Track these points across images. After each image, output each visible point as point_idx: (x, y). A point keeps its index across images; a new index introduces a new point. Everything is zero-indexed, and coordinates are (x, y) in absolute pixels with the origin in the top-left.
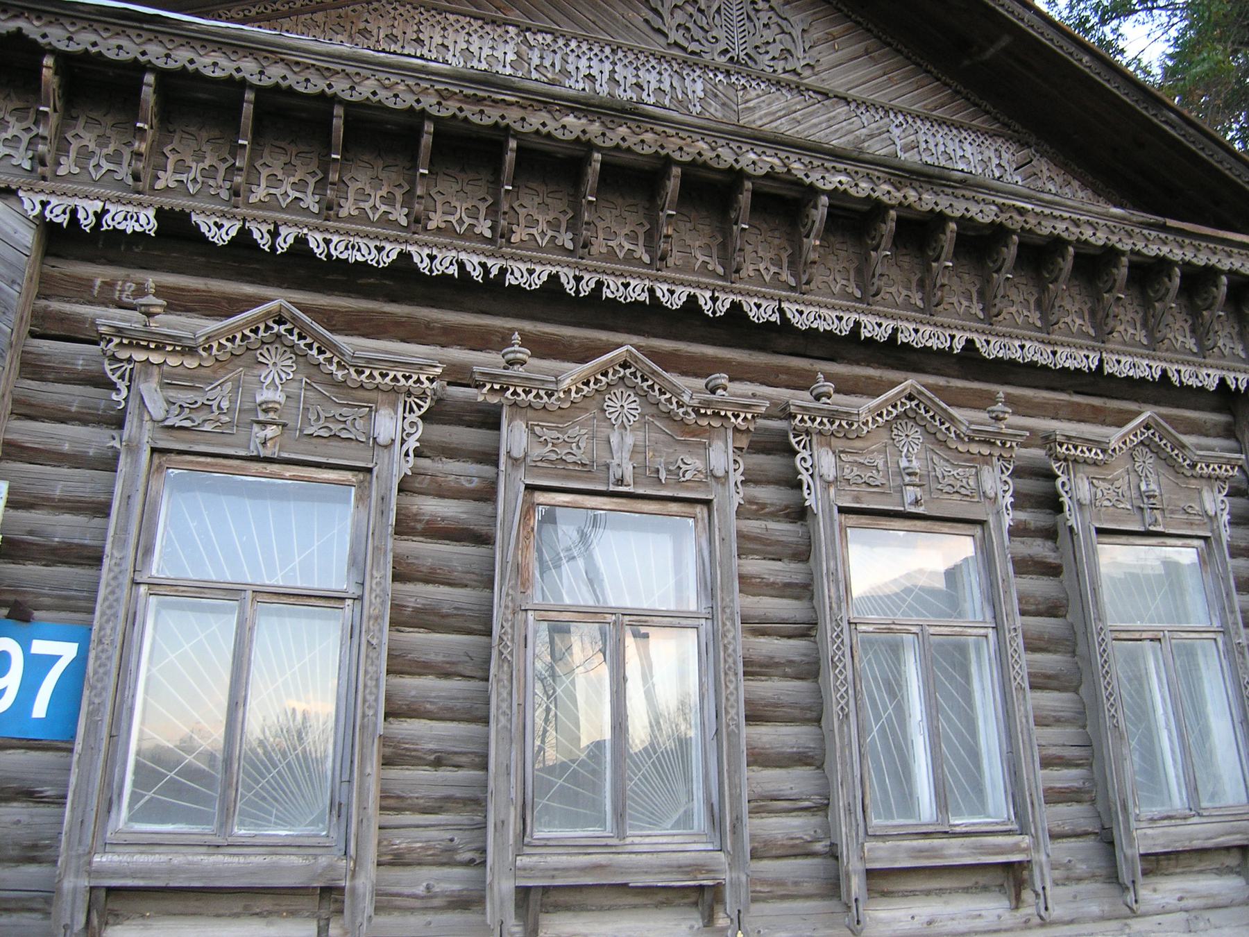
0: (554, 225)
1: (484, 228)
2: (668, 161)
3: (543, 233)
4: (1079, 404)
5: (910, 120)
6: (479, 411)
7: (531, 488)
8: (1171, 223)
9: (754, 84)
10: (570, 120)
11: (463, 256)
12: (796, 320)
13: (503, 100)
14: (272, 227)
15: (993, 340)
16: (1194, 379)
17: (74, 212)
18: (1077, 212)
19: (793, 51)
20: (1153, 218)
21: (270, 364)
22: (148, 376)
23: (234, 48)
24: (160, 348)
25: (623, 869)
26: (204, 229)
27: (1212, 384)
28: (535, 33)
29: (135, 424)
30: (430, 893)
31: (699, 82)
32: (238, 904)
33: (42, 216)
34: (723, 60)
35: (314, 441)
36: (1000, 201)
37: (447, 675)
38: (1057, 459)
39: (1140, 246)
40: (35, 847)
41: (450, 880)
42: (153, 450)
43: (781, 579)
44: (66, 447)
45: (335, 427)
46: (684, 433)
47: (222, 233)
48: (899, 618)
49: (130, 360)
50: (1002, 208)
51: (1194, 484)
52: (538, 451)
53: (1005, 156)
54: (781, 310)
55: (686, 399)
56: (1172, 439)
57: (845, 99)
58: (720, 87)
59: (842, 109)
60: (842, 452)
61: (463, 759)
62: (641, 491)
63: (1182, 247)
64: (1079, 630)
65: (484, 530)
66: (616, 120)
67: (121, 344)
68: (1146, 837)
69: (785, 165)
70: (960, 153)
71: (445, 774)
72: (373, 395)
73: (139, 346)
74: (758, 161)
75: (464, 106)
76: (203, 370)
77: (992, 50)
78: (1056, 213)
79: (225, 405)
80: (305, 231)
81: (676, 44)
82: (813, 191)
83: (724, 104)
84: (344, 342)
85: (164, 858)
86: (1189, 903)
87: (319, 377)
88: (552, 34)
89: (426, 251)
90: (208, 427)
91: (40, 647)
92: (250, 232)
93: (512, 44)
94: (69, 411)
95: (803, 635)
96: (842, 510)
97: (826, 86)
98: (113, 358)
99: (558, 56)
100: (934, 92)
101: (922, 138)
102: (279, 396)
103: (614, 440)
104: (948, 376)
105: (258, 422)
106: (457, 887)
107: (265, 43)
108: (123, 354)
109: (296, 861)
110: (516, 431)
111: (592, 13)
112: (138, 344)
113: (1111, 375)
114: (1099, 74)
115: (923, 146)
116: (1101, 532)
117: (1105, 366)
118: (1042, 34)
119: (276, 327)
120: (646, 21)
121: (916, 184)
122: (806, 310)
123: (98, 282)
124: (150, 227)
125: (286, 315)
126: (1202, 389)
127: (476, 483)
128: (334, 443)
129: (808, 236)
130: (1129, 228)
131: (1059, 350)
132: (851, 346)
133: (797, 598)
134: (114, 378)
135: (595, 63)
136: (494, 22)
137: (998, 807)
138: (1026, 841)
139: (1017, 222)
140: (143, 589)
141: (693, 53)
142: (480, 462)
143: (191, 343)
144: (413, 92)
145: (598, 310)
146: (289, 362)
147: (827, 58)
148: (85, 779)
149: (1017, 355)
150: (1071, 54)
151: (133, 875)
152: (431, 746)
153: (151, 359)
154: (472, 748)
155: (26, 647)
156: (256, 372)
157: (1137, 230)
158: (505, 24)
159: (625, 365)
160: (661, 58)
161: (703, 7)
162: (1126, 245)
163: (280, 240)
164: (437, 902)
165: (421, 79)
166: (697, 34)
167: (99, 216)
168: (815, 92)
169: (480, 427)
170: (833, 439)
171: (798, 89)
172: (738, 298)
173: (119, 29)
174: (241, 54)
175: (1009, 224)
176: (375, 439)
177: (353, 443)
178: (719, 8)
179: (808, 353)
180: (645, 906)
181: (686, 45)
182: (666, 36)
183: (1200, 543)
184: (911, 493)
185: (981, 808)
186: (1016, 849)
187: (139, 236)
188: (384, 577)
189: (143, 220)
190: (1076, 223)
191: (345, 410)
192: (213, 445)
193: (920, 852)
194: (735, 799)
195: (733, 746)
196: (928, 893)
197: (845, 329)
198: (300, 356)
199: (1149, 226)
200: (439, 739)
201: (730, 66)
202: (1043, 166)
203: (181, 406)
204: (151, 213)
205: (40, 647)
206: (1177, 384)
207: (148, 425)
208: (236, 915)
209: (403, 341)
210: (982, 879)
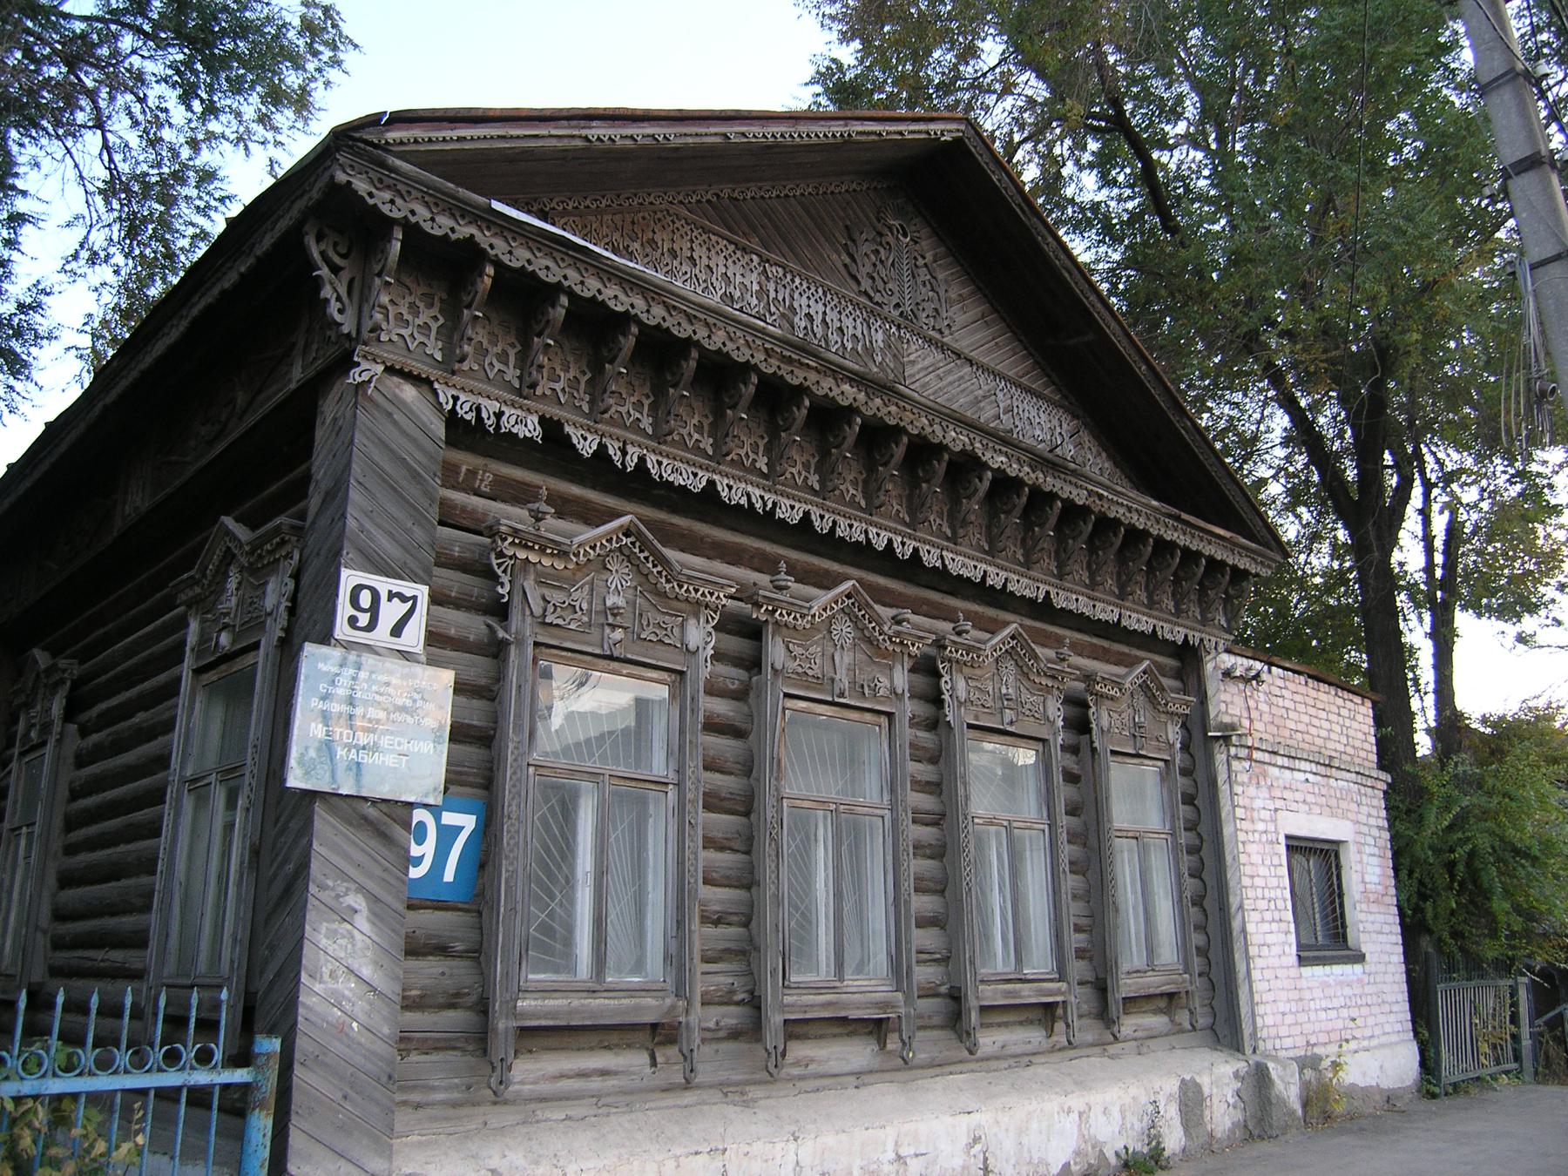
0: (806, 466)
7: (786, 695)
10: (846, 387)
11: (750, 488)
17: (478, 410)
24: (542, 550)
25: (845, 1006)
26: (575, 441)
30: (718, 1027)
32: (594, 1039)
33: (453, 411)
37: (722, 849)
40: (457, 995)
41: (731, 1016)
42: (536, 644)
43: (925, 778)
44: (453, 631)
45: (661, 633)
47: (587, 446)
48: (997, 814)
50: (1090, 493)
51: (1163, 718)
52: (792, 665)
53: (1065, 426)
55: (886, 628)
59: (967, 369)
61: (735, 918)
62: (853, 703)
64: (755, 751)
65: (744, 726)
67: (512, 543)
68: (537, 995)
71: (722, 930)
72: (683, 606)
73: (526, 547)
74: (957, 439)
81: (866, 293)
82: (985, 466)
84: (671, 554)
85: (565, 1002)
86: (1139, 1034)
87: (647, 586)
89: (726, 481)
91: (449, 818)
93: (755, 275)
95: (935, 824)
96: (970, 726)
98: (501, 555)
100: (1024, 359)
102: (621, 602)
103: (837, 658)
106: (734, 1021)
107: (656, 286)
109: (650, 1001)
116: (1113, 753)
120: (845, 266)
123: (464, 469)
126: (1174, 642)
127: (735, 686)
128: (659, 647)
133: (931, 793)
134: (499, 572)
135: (812, 302)
137: (1040, 961)
138: (1063, 986)
139: (1097, 506)
140: (531, 769)
145: (831, 545)
148: (166, 924)
149: (1073, 607)
151: (546, 1016)
152: (717, 908)
154: (742, 909)
155: (438, 819)
159: (849, 596)
160: (857, 305)
164: (721, 1034)
173: (548, 250)
180: (841, 1035)
182: (859, 283)
183: (1161, 764)
184: (1009, 715)
185: (639, 966)
186: (1059, 992)
188: (696, 767)
190: (1130, 509)
192: (575, 642)
193: (1008, 994)
194: (909, 951)
195: (908, 910)
196: (999, 1025)
198: (637, 567)
199: (1170, 516)
200: (721, 902)
202: (1085, 436)
205: (449, 818)
207: (529, 620)
208: (592, 1049)
210: (1031, 1015)
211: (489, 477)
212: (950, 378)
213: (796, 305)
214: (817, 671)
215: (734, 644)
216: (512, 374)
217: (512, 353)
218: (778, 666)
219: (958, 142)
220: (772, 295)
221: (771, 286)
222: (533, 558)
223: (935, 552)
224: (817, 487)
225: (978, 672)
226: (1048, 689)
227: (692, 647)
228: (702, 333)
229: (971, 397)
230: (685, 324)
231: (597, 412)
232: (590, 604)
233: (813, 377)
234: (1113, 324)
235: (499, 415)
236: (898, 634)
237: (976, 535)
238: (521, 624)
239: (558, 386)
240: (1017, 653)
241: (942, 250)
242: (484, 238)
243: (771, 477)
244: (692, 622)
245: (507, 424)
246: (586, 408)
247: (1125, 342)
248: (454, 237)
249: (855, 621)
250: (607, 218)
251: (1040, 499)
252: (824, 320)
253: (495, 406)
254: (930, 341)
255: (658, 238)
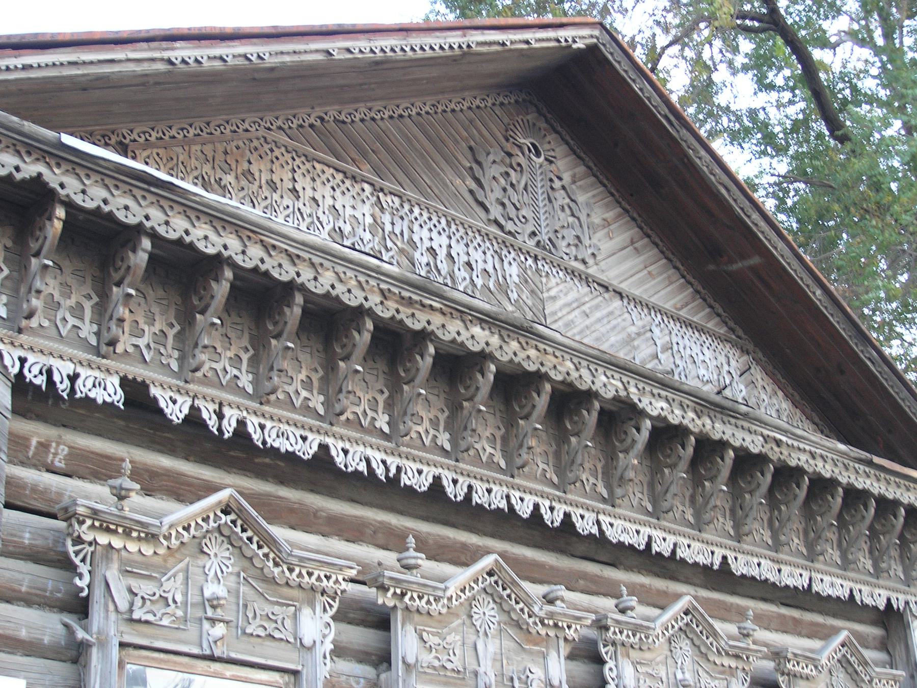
0: (435, 423)
1: (382, 422)
2: (545, 377)
3: (427, 432)
4: (784, 616)
5: (665, 319)
6: (362, 609)
8: (877, 460)
9: (554, 270)
10: (476, 330)
12: (610, 534)
13: (431, 306)
14: (217, 407)
15: (739, 556)
16: (701, 556)
17: (50, 373)
18: (774, 423)
19: (582, 237)
20: (864, 455)
21: (212, 554)
22: (107, 559)
23: (223, 224)
24: (127, 533)
26: (162, 404)
27: (881, 604)
28: (385, 195)
29: (102, 615)
31: (514, 264)
33: (20, 375)
34: (531, 243)
35: (252, 640)
36: (766, 432)
38: (783, 674)
39: (852, 480)
42: (122, 645)
44: (23, 634)
45: (270, 626)
46: (529, 642)
49: (94, 543)
50: (766, 439)
52: (427, 658)
54: (598, 523)
55: (536, 609)
56: (631, 626)
57: (620, 294)
58: (529, 272)
59: (617, 303)
60: (637, 663)
63: (878, 480)
66: (511, 334)
69: (626, 389)
70: (701, 357)
72: (296, 593)
73: (108, 530)
75: (401, 308)
76: (156, 558)
77: (740, 265)
78: (802, 446)
79: (179, 598)
80: (245, 414)
81: (496, 222)
82: (642, 413)
83: (532, 292)
84: (280, 532)
87: (252, 571)
88: (400, 197)
90: (165, 622)
92: (199, 410)
94: (20, 592)
97: (603, 277)
98: (78, 541)
99: (406, 223)
100: (681, 289)
101: (674, 340)
104: (695, 585)
105: (208, 619)
108: (88, 537)
110: (408, 634)
111: (429, 178)
112: (108, 527)
113: (480, 507)
114: (826, 308)
115: (675, 347)
117: (654, 544)
118: (789, 264)
119: (223, 516)
120: (471, 192)
121: (712, 414)
122: (310, 436)
124: (116, 398)
125: (233, 505)
128: (269, 643)
129: (626, 451)
130: (846, 461)
131: (783, 567)
132: (647, 559)
134: (77, 561)
135: (434, 235)
136: (354, 178)
139: (774, 454)
141: (510, 233)
142: (360, 661)
143: (153, 530)
144: (363, 290)
145: (468, 514)
146: (227, 554)
147: (606, 246)
150: (808, 286)
153: (113, 544)
156: (201, 563)
157: (851, 464)
158: (363, 181)
159: (490, 574)
161: (514, 182)
162: (844, 480)
163: (225, 422)
165: (369, 276)
166: (513, 213)
167: (73, 378)
168: (599, 284)
169: (358, 625)
170: (631, 651)
171: (587, 280)
172: (568, 509)
174: (228, 229)
175: (770, 454)
176: (300, 639)
177: (283, 643)
178: (526, 185)
179: (596, 558)
181: (503, 222)
182: (487, 210)
187: (108, 406)
189: (111, 390)
190: (813, 456)
191: (277, 609)
197: (307, 450)
199: (860, 461)
201: (538, 251)
202: (757, 373)
203: (143, 598)
204: (116, 381)
206: (383, 478)
209: (293, 528)
211: (64, 450)
212: (598, 315)
213: (416, 238)
214: (457, 663)
215: (360, 636)
216: (88, 330)
217: (88, 306)
218: (411, 660)
219: (593, 50)
220: (388, 228)
221: (387, 219)
222: (117, 543)
223: (590, 517)
224: (447, 446)
225: (648, 655)
226: (732, 671)
227: (307, 642)
228: (306, 275)
229: (624, 335)
230: (287, 265)
231: (188, 370)
232: (185, 594)
233: (437, 320)
234: (781, 245)
235: (73, 378)
236: (551, 615)
237: (637, 495)
238: (104, 622)
239: (142, 342)
240: (692, 630)
241: (581, 169)
242: (53, 177)
243: (393, 437)
244: (306, 612)
245: (83, 388)
246: (175, 366)
247: (795, 264)
248: (18, 176)
249: (499, 602)
250: (196, 148)
251: (708, 449)
252: (449, 255)
253: (68, 368)
254: (573, 273)
255: (254, 169)
